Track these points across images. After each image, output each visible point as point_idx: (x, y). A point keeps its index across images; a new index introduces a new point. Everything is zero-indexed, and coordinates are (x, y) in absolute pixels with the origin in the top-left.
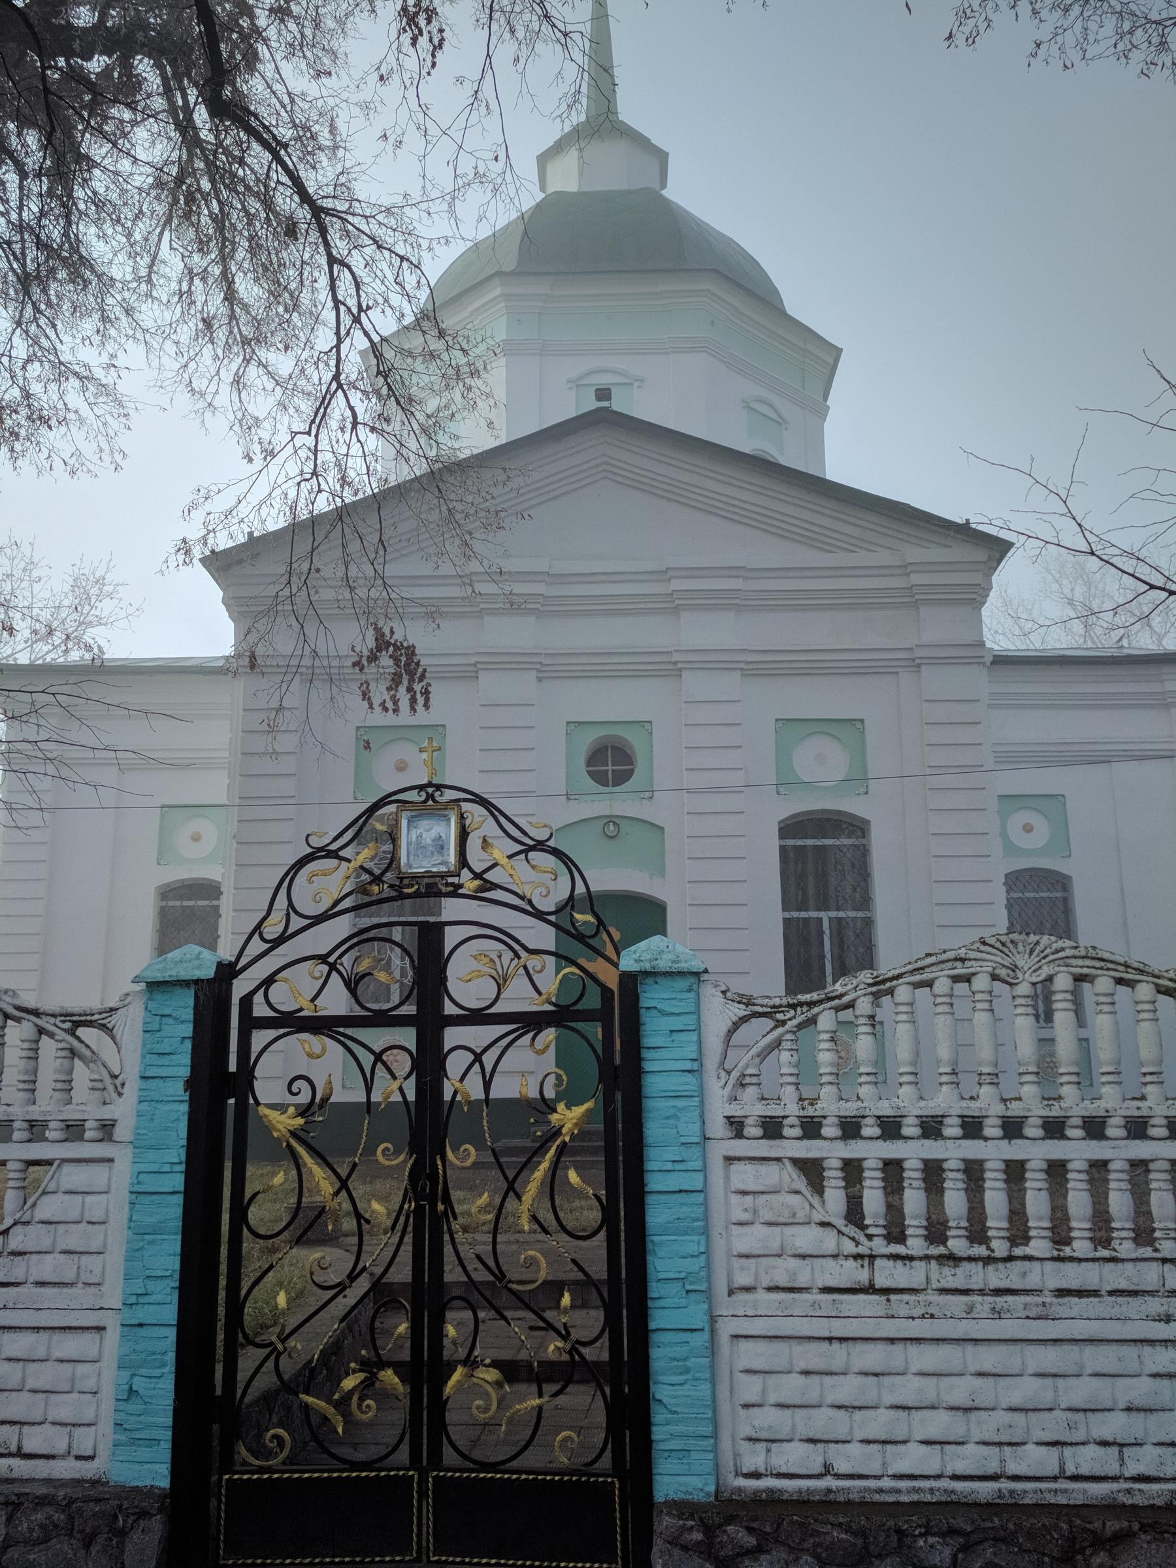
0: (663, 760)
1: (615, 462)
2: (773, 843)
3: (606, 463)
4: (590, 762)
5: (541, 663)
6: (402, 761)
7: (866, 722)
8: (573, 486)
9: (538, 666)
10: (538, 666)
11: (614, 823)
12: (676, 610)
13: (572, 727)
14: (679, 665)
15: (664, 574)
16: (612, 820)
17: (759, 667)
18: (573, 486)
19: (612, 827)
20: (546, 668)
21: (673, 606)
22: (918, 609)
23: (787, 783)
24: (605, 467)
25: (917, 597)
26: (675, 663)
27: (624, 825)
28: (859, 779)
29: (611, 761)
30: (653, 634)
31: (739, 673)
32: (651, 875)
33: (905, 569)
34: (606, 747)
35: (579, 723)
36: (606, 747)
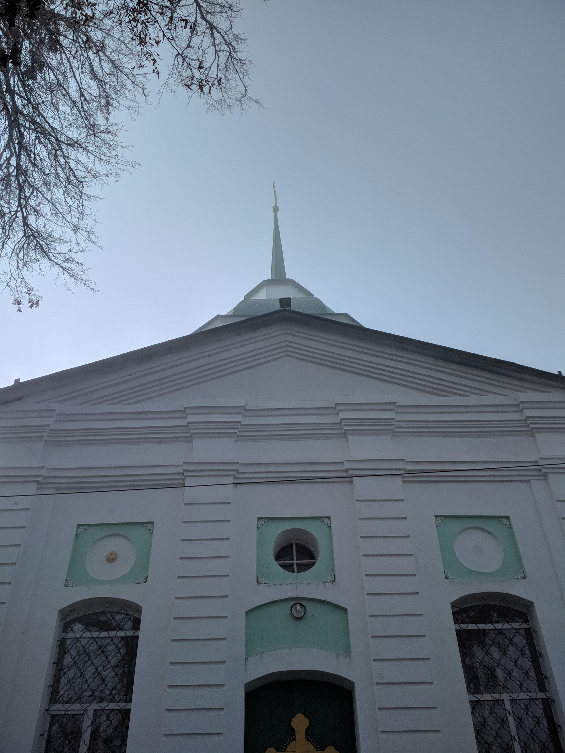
0: (341, 548)
1: (292, 344)
2: (449, 628)
3: (287, 346)
4: (278, 557)
5: (237, 471)
6: (112, 554)
7: (511, 518)
8: (264, 360)
9: (235, 473)
10: (235, 473)
11: (301, 605)
12: (344, 435)
13: (262, 522)
14: (351, 472)
15: (335, 409)
16: (298, 601)
17: (413, 475)
18: (264, 360)
19: (298, 607)
20: (243, 478)
21: (342, 432)
22: (533, 436)
23: (453, 569)
24: (287, 343)
25: (532, 426)
26: (347, 471)
27: (310, 608)
28: (516, 565)
29: (296, 552)
30: (328, 452)
31: (399, 479)
32: (338, 655)
33: (518, 407)
34: (291, 545)
35: (268, 519)
36: (291, 545)
